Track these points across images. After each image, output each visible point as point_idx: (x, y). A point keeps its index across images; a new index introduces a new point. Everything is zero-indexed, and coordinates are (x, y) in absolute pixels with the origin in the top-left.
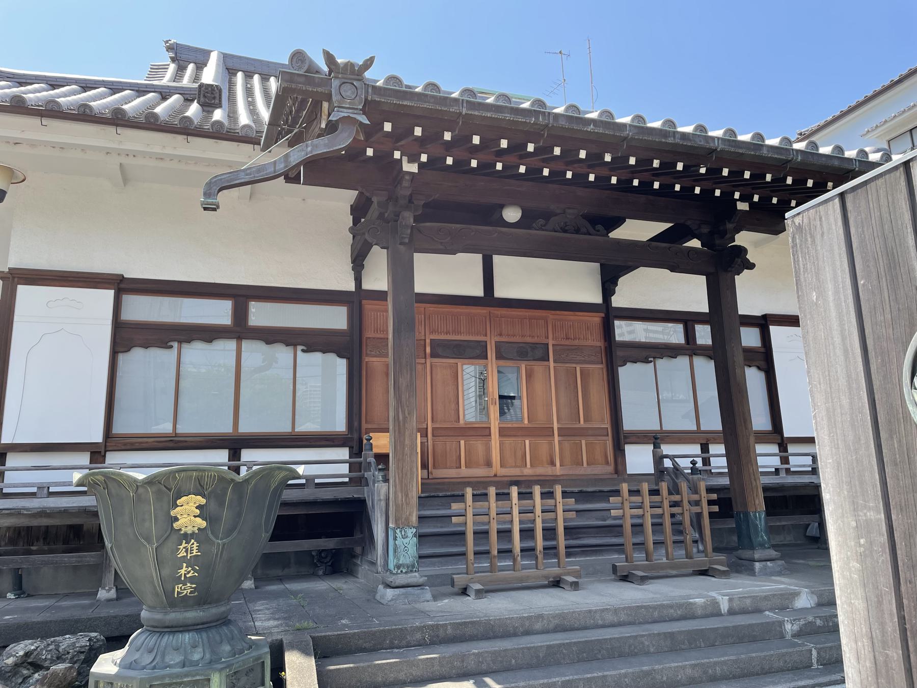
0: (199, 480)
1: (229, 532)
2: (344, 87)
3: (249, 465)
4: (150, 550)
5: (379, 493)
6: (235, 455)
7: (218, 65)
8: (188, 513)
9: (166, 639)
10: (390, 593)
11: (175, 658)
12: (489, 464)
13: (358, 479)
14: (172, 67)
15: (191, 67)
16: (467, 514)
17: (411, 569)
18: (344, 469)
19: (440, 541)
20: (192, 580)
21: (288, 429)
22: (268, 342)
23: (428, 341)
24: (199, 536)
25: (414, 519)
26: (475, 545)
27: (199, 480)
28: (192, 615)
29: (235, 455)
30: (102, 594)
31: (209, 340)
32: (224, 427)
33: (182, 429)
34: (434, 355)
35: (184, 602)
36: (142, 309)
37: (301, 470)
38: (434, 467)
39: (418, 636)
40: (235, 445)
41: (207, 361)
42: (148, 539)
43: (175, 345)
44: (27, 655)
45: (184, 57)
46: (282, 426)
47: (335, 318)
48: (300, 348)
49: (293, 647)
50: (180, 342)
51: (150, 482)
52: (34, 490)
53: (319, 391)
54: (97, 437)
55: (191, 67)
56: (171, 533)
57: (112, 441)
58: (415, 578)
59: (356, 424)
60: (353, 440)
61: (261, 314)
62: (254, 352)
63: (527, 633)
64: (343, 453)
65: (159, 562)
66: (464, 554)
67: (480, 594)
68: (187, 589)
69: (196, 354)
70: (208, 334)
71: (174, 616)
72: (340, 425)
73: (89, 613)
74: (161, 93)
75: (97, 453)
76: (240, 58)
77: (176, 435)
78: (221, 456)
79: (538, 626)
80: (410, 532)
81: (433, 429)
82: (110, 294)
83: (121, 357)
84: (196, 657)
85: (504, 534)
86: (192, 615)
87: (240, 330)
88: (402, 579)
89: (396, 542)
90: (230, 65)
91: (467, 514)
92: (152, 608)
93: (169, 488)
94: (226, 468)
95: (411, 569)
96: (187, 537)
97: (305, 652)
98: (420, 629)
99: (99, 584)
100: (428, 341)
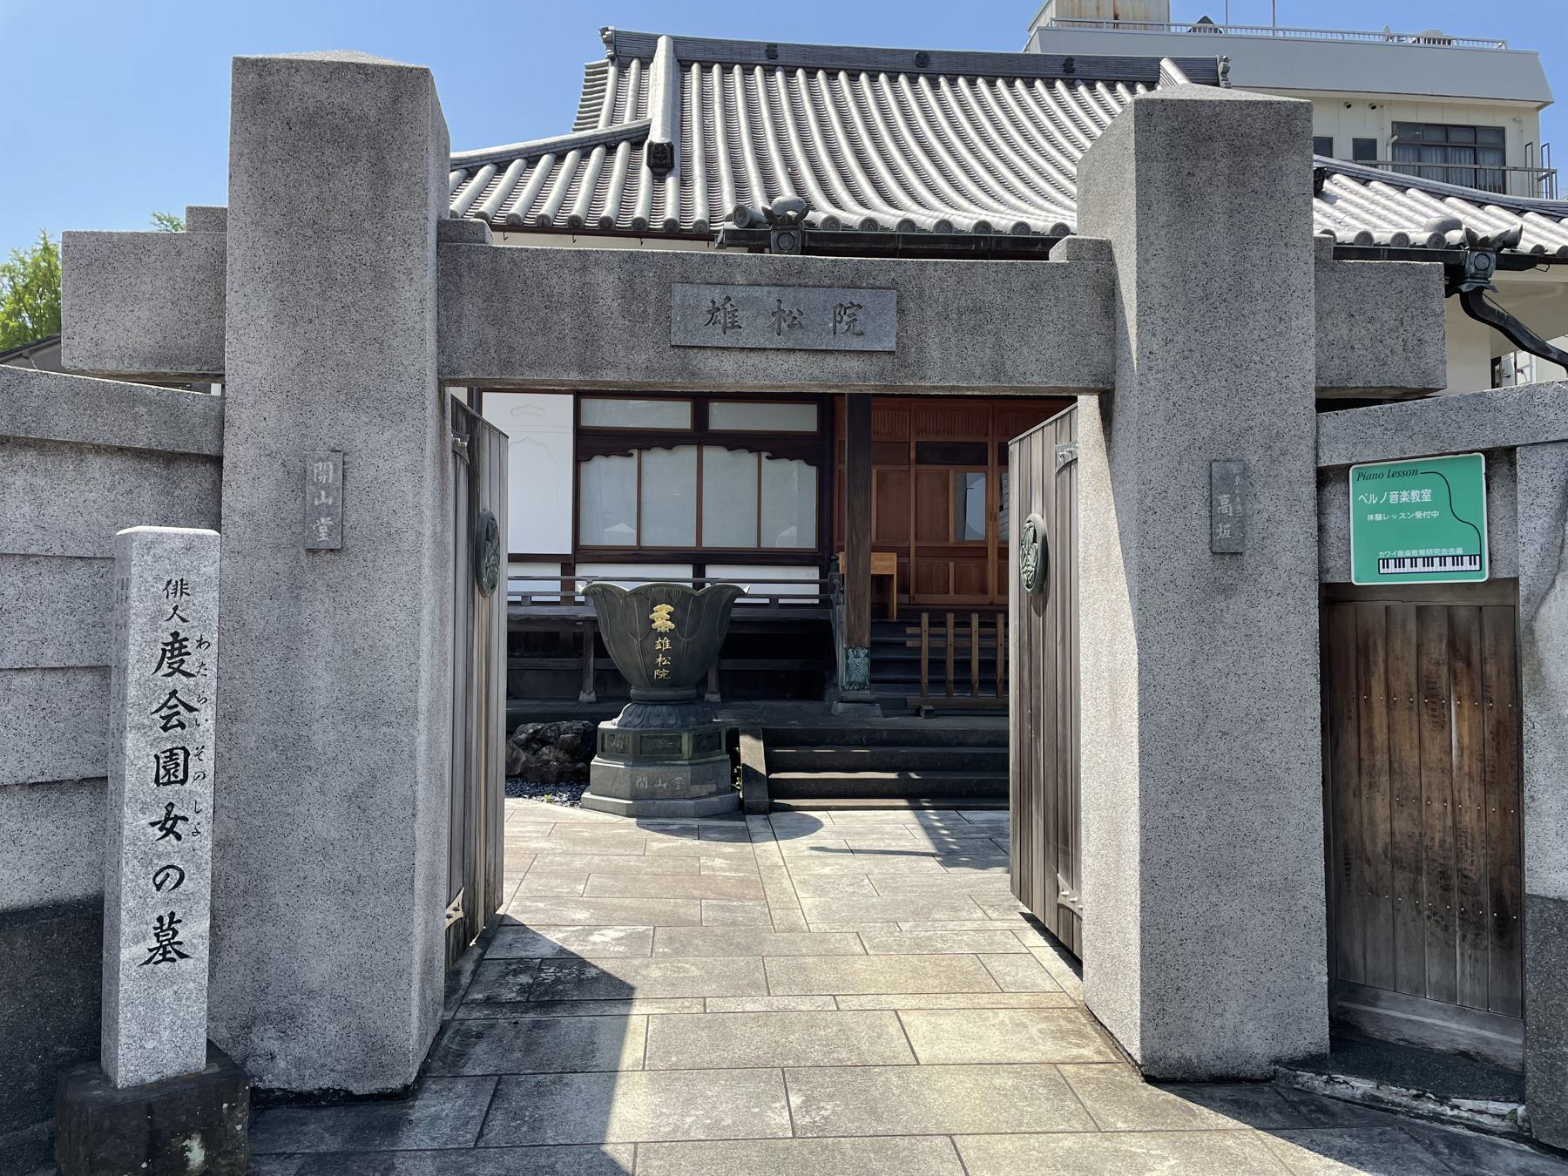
0: (669, 593)
1: (690, 635)
2: (783, 238)
3: (711, 581)
4: (636, 642)
5: (841, 613)
6: (699, 572)
7: (667, 57)
8: (662, 616)
9: (649, 709)
10: (841, 707)
11: (656, 722)
12: (983, 590)
13: (825, 602)
14: (612, 70)
15: (634, 64)
16: (921, 638)
17: (862, 686)
18: (814, 589)
19: (889, 665)
20: (666, 667)
21: (753, 544)
22: (730, 448)
23: (913, 445)
24: (669, 634)
25: (867, 640)
26: (930, 673)
27: (669, 593)
28: (669, 693)
29: (699, 572)
30: (583, 697)
31: (669, 447)
32: (689, 542)
33: (648, 542)
34: (919, 461)
35: (660, 684)
36: (606, 414)
37: (746, 588)
38: (917, 591)
39: (857, 737)
40: (699, 559)
41: (669, 470)
42: (635, 636)
43: (635, 452)
44: (536, 732)
45: (625, 50)
46: (747, 542)
47: (804, 420)
48: (764, 455)
49: (745, 733)
50: (640, 449)
51: (635, 593)
52: (519, 599)
53: (787, 502)
54: (568, 550)
55: (634, 64)
56: (651, 633)
57: (582, 553)
58: (866, 694)
59: (827, 541)
60: (822, 557)
61: (722, 418)
62: (715, 456)
63: (960, 744)
64: (813, 573)
65: (643, 652)
66: (918, 682)
67: (929, 714)
68: (663, 674)
69: (656, 460)
70: (666, 440)
71: (654, 693)
72: (809, 542)
73: (576, 710)
74: (605, 144)
75: (568, 564)
76: (694, 40)
77: (641, 548)
78: (685, 572)
79: (973, 740)
80: (863, 653)
81: (917, 548)
82: (571, 397)
83: (583, 466)
84: (672, 722)
85: (962, 665)
86: (669, 693)
87: (700, 435)
88: (853, 695)
89: (852, 663)
90: (683, 55)
91: (921, 638)
92: (638, 687)
93: (649, 596)
94: (690, 585)
95: (862, 686)
96: (662, 635)
97: (756, 737)
98: (859, 731)
99: (580, 688)
100: (913, 445)
